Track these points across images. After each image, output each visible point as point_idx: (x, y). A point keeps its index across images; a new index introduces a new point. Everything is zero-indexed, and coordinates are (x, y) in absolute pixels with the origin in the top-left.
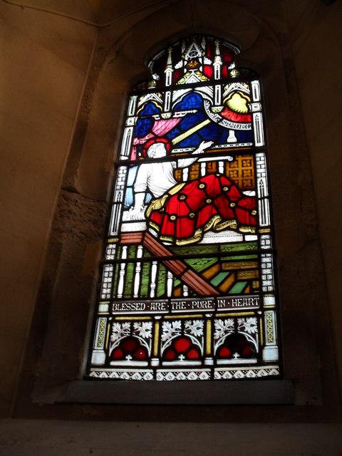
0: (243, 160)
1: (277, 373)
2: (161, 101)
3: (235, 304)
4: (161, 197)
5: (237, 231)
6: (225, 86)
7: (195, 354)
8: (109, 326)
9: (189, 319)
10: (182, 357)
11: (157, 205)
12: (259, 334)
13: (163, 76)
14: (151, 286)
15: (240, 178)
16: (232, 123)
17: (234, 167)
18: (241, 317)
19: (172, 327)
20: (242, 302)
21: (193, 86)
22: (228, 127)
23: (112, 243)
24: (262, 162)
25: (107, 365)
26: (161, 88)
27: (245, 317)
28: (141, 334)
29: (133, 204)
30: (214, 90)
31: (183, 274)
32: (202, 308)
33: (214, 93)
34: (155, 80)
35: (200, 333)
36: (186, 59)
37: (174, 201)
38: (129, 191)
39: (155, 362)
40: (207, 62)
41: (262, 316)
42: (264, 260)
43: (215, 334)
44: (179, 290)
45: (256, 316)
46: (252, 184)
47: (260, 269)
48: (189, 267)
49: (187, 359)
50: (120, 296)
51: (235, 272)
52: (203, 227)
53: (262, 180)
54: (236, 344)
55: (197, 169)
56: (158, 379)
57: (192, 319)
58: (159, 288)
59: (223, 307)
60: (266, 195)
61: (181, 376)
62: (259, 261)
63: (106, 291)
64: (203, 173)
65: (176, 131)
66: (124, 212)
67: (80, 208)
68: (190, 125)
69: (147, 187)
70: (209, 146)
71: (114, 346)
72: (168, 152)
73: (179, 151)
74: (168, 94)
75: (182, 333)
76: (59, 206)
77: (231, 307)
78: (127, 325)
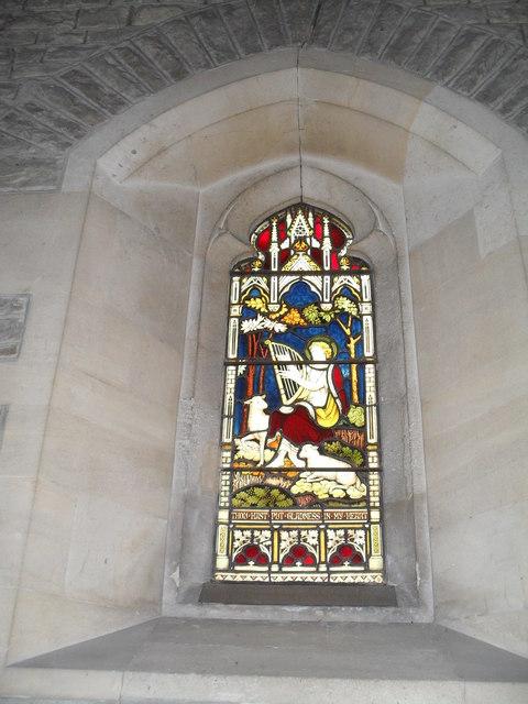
2: (357, 287)
13: (268, 256)
21: (302, 273)
26: (265, 270)
27: (355, 529)
40: (316, 244)
41: (369, 529)
54: (346, 553)
66: (315, 359)
74: (274, 280)
78: (294, 533)
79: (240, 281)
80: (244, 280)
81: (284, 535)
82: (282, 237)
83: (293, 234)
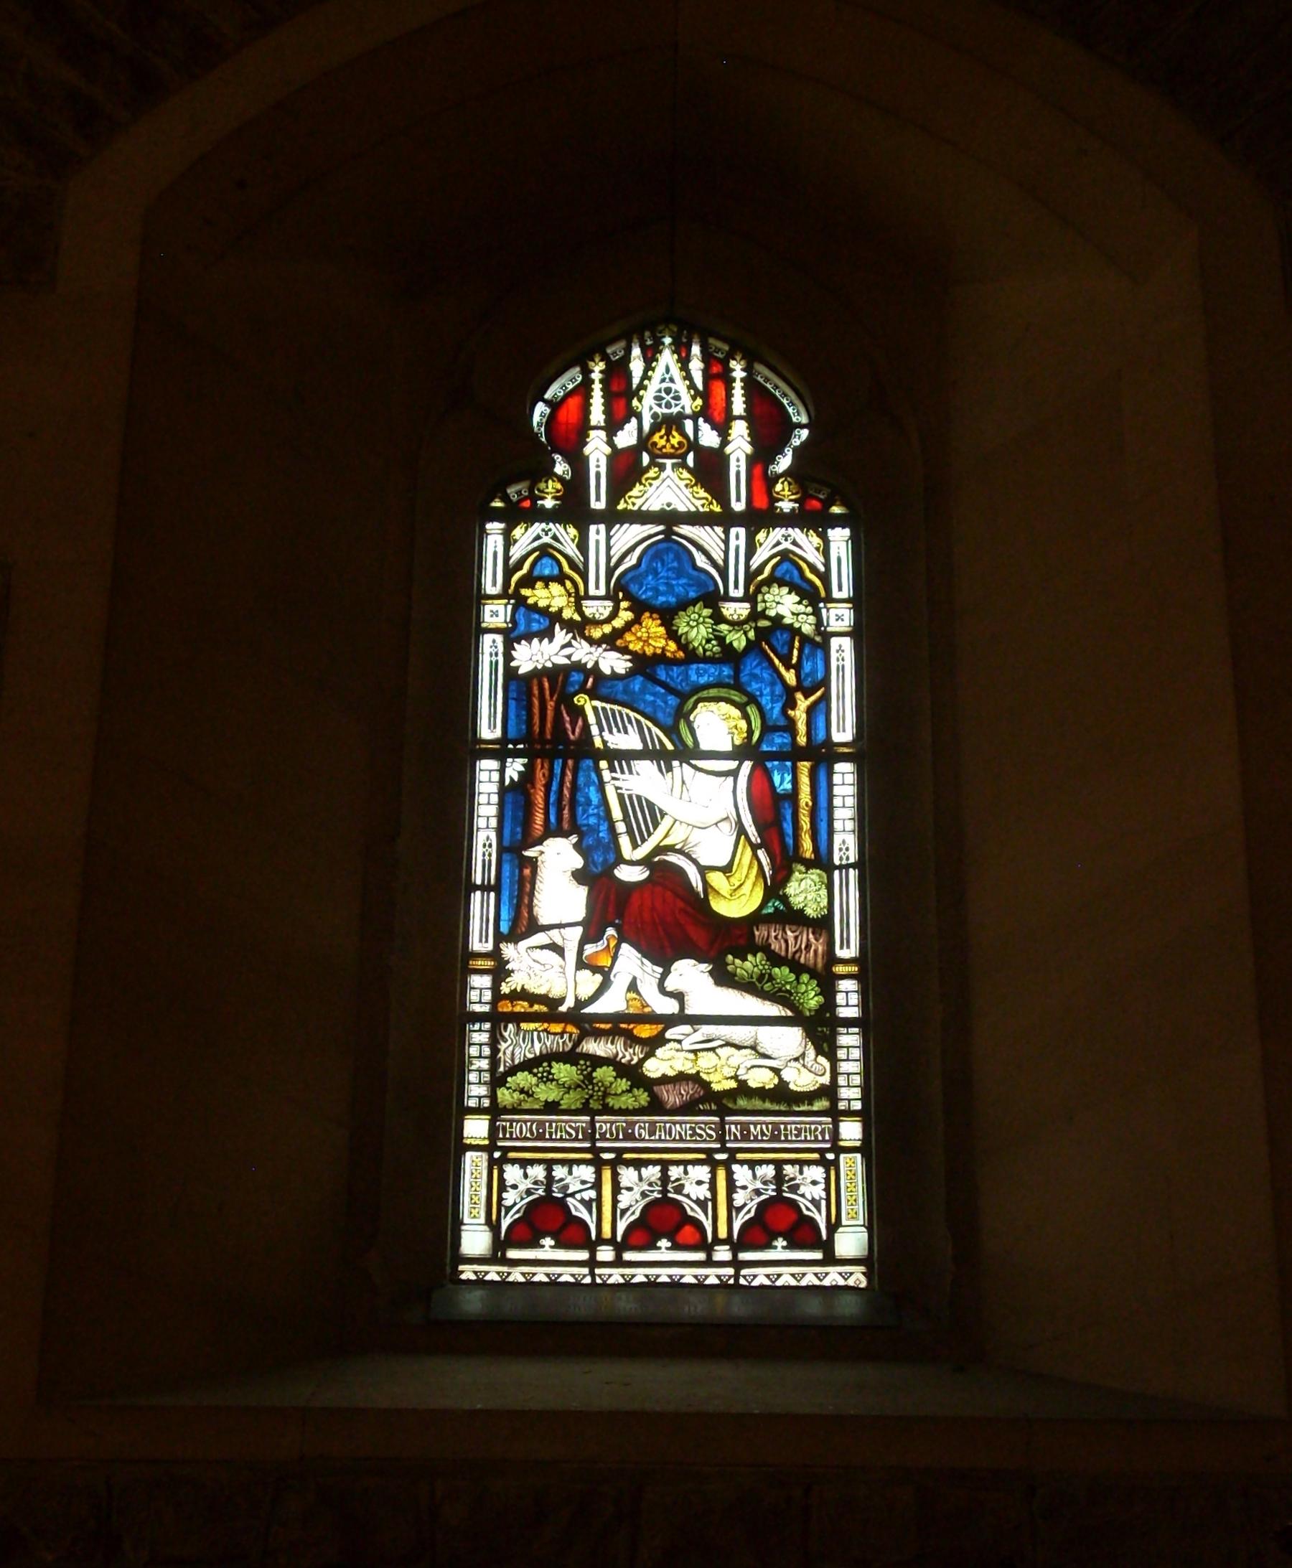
12: (828, 1200)
13: (579, 464)
19: (526, 1176)
21: (669, 518)
25: (497, 1256)
27: (802, 1163)
28: (802, 1190)
30: (726, 542)
33: (726, 552)
34: (561, 479)
40: (709, 438)
41: (836, 1163)
43: (735, 1196)
45: (822, 1162)
49: (559, 1245)
59: (736, 1140)
83: (647, 406)
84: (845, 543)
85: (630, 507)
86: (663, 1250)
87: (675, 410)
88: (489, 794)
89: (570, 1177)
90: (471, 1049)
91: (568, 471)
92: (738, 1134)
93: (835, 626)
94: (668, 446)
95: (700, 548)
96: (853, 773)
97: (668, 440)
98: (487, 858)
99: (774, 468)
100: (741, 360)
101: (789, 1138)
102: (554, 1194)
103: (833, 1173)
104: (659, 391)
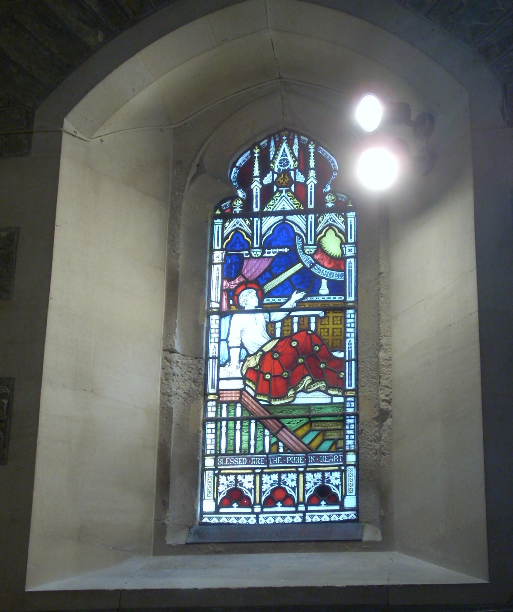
0: (334, 317)
1: (355, 517)
2: (249, 231)
3: (322, 460)
4: (256, 354)
5: (326, 392)
6: (319, 217)
7: (290, 502)
8: (216, 478)
9: (284, 472)
10: (279, 504)
11: (253, 362)
13: (249, 193)
14: (251, 443)
15: (330, 337)
16: (325, 270)
17: (325, 324)
18: (328, 471)
19: (270, 479)
20: (328, 458)
21: (284, 213)
22: (321, 275)
23: (212, 400)
24: (352, 330)
25: (217, 512)
27: (331, 471)
29: (229, 360)
30: (307, 222)
31: (278, 432)
32: (295, 463)
33: (307, 226)
34: (242, 199)
35: (294, 484)
36: (276, 170)
37: (268, 357)
38: (223, 344)
39: (257, 509)
40: (300, 178)
41: (345, 471)
42: (348, 421)
43: (306, 485)
44: (275, 446)
45: (339, 470)
46: (341, 344)
47: (344, 430)
48: (284, 426)
49: (327, 504)
50: (223, 452)
51: (323, 432)
52: (295, 388)
53: (351, 342)
55: (290, 324)
56: (260, 523)
57: (287, 472)
58: (258, 444)
59: (313, 462)
60: (353, 358)
61: (279, 520)
62: (343, 422)
63: (210, 447)
64: (296, 330)
65: (268, 275)
67: (181, 368)
68: (282, 269)
69: (241, 341)
70: (302, 297)
71: (222, 496)
72: (261, 303)
73: (271, 300)
75: (279, 484)
76: (163, 369)
77: (320, 463)
78: (232, 478)
79: (223, 225)
80: (227, 224)
81: (265, 478)
82: (265, 170)
83: (276, 166)
84: (353, 218)
85: (269, 210)
86: (235, 507)
87: (286, 168)
88: (215, 329)
89: (331, 477)
90: (354, 427)
91: (245, 195)
92: (314, 460)
93: (348, 254)
94: (284, 182)
95: (296, 225)
96: (354, 314)
97: (284, 180)
98: (350, 349)
99: (325, 190)
100: (313, 144)
101: (324, 461)
102: (281, 485)
103: (344, 474)
104: (281, 160)
